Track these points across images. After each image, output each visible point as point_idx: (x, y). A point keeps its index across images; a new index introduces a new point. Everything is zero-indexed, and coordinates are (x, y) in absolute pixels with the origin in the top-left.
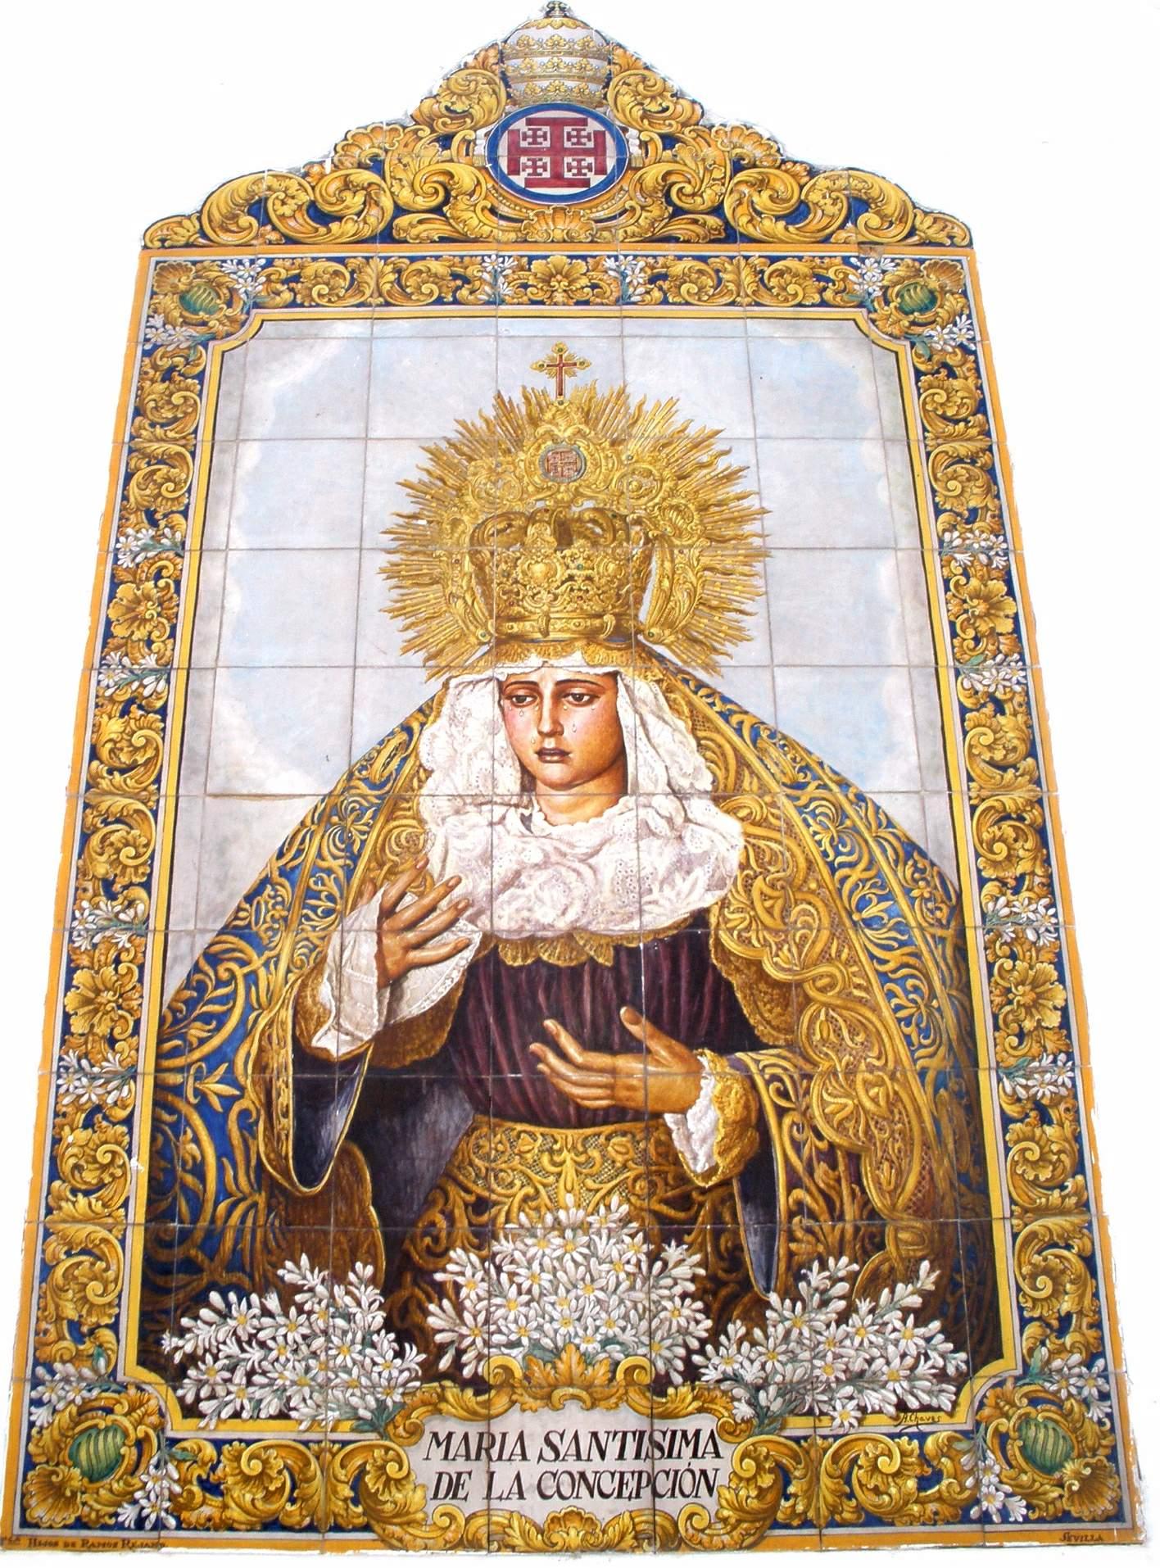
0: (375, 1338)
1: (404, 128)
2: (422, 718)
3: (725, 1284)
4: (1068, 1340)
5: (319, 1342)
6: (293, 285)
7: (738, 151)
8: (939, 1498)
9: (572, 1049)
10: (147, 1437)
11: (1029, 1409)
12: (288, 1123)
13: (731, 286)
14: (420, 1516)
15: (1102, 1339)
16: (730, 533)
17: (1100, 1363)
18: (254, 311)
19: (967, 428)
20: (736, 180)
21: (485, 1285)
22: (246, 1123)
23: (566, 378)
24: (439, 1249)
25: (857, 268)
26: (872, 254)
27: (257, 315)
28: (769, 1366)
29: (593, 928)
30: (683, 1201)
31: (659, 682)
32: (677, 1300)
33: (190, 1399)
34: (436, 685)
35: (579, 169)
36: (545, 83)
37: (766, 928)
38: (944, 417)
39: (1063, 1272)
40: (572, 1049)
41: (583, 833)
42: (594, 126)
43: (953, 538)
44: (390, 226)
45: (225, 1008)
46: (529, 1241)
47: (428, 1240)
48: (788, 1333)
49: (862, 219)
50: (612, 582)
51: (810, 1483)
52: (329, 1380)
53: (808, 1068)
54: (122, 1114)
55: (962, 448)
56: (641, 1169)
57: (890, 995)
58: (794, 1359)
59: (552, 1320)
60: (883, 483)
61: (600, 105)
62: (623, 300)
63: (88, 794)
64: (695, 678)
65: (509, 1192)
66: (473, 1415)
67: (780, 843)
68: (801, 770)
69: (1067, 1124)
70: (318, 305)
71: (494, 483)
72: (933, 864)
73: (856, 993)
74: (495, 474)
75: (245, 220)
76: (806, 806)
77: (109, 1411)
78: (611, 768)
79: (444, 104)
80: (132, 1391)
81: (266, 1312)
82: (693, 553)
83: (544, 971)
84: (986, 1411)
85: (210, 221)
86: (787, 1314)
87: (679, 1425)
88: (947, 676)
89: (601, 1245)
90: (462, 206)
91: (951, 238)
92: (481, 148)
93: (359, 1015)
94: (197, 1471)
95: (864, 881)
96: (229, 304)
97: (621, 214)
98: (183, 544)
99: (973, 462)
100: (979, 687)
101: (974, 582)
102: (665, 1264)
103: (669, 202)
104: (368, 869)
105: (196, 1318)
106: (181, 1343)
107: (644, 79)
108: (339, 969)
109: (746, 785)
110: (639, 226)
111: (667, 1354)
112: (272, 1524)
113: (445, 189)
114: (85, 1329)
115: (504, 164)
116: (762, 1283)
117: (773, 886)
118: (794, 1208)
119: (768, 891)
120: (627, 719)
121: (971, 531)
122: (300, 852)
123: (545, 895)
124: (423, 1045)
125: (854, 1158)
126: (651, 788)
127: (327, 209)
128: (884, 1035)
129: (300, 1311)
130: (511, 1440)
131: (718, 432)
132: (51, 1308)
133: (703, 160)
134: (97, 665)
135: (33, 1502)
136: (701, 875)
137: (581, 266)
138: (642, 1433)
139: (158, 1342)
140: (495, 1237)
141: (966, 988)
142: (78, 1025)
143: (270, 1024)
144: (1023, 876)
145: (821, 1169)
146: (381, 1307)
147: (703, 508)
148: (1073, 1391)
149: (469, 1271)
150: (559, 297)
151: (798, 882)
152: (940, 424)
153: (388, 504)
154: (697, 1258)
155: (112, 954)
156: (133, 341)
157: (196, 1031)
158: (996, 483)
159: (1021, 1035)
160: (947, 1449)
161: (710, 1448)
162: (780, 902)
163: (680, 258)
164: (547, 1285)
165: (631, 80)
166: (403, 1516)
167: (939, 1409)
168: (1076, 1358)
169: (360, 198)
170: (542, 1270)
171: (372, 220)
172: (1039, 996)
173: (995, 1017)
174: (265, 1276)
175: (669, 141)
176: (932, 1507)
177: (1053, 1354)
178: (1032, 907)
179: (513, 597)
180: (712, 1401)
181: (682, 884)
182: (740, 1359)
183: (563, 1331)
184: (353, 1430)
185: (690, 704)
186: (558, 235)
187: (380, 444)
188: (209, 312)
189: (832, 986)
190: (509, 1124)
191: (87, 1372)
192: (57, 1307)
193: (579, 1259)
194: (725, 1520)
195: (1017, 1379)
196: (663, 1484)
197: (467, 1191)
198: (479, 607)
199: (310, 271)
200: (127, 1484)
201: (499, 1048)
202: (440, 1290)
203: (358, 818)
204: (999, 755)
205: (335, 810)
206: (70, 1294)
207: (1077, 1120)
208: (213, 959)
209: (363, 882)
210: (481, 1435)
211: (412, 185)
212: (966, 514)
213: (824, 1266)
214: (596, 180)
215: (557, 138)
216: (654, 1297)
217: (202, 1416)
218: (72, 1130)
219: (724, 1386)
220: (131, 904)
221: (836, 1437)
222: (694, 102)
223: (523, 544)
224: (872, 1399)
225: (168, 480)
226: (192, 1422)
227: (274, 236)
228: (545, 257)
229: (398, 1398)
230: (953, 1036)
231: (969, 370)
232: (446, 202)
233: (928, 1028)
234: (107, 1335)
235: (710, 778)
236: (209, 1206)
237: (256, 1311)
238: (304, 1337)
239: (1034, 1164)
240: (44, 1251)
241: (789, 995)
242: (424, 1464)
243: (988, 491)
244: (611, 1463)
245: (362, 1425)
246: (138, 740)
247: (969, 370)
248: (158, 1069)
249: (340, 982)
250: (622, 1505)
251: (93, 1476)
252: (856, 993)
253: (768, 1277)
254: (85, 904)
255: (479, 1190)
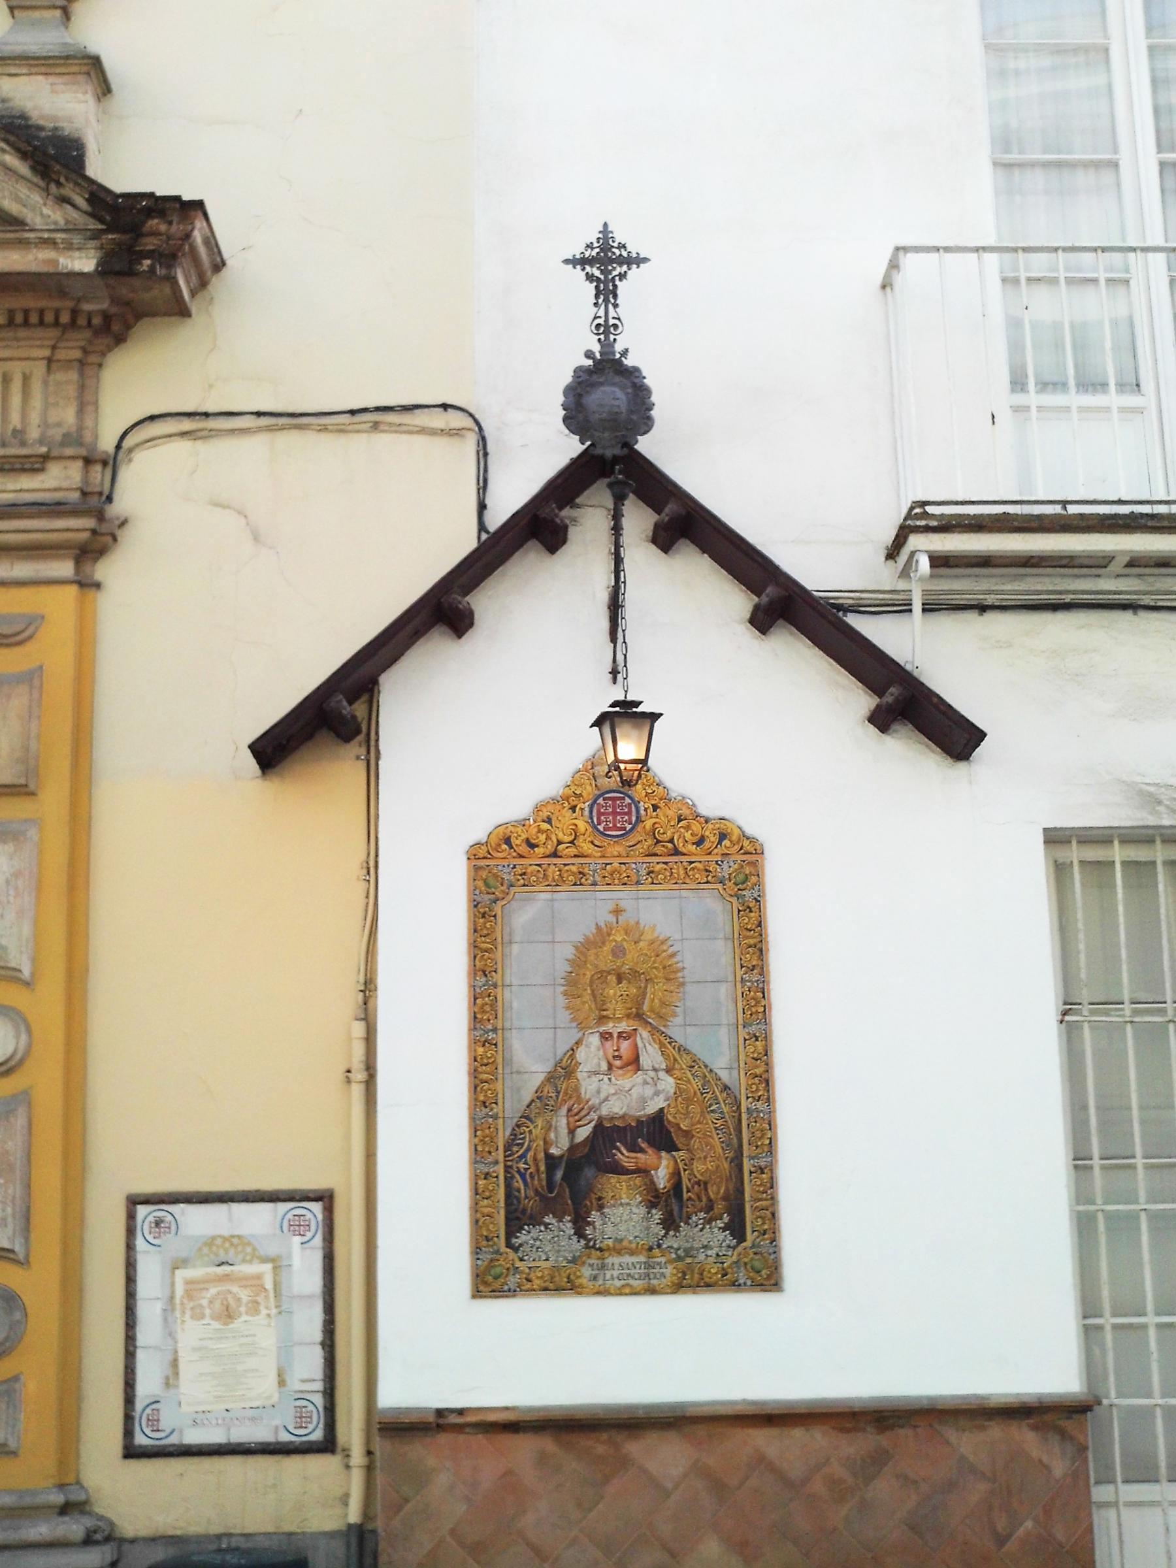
9: (625, 1152)
12: (544, 1176)
27: (513, 890)
34: (580, 1034)
40: (625, 1152)
43: (746, 977)
55: (752, 941)
62: (638, 883)
63: (474, 1073)
74: (597, 955)
75: (505, 846)
78: (634, 1062)
92: (586, 813)
112: (546, 1289)
120: (640, 1044)
125: (706, 1183)
136: (662, 1097)
145: (696, 1187)
153: (562, 968)
156: (469, 901)
157: (515, 1149)
166: (581, 1286)
169: (544, 836)
179: (604, 1003)
181: (656, 1099)
186: (616, 853)
196: (652, 1276)
198: (593, 1006)
202: (589, 1224)
205: (552, 1077)
208: (518, 1126)
224: (709, 1253)
241: (688, 1134)
242: (587, 1272)
245: (569, 1262)
251: (496, 1278)
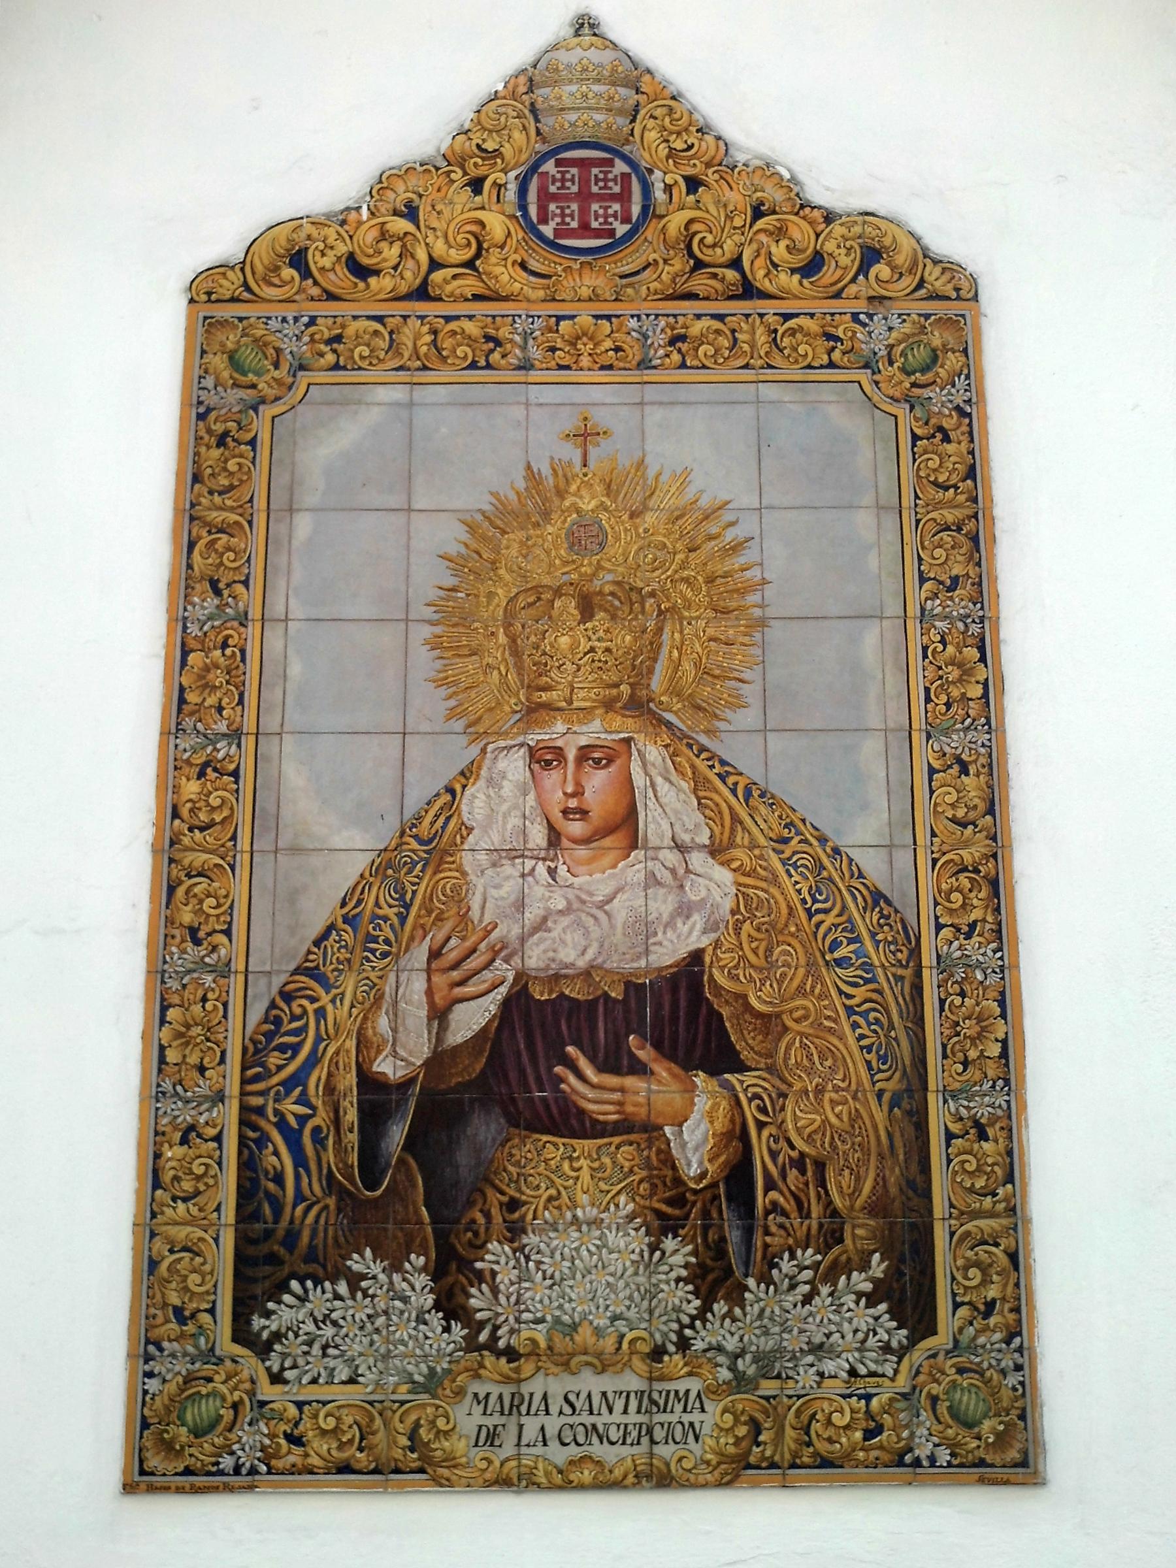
0: (427, 1316)
1: (437, 169)
2: (463, 781)
3: (713, 1270)
4: (992, 1321)
5: (381, 1321)
6: (335, 346)
7: (759, 194)
8: (881, 1447)
10: (241, 1400)
11: (957, 1377)
12: (353, 1138)
13: (746, 347)
14: (464, 1460)
15: (1019, 1321)
16: (734, 604)
17: (1017, 1340)
18: (300, 373)
19: (956, 494)
20: (755, 228)
21: (516, 1272)
22: (318, 1138)
23: (590, 448)
24: (479, 1243)
25: (864, 325)
26: (881, 309)
27: (304, 378)
28: (746, 1338)
29: (607, 966)
30: (678, 1201)
31: (666, 746)
32: (673, 1284)
33: (276, 1369)
34: (475, 750)
35: (606, 217)
36: (573, 117)
37: (752, 966)
38: (935, 484)
39: (990, 1265)
40: (589, 1072)
41: (600, 883)
42: (620, 167)
43: (935, 606)
44: (425, 282)
45: (297, 1039)
46: (552, 1235)
47: (470, 1234)
48: (762, 1311)
49: (873, 271)
50: (628, 653)
51: (777, 1434)
52: (389, 1351)
53: (784, 1087)
54: (211, 1132)
55: (950, 516)
56: (644, 1173)
57: (855, 1026)
58: (766, 1333)
59: (571, 1300)
60: (875, 551)
61: (627, 142)
62: (644, 364)
64: (697, 742)
65: (536, 1195)
66: (506, 1380)
67: (766, 891)
68: (786, 826)
69: (1001, 1140)
70: (360, 368)
71: (525, 557)
72: (896, 911)
73: (826, 1023)
74: (526, 548)
75: (288, 273)
76: (789, 859)
77: (209, 1380)
78: (624, 827)
79: (474, 142)
80: (228, 1363)
81: (337, 1297)
82: (701, 624)
83: (566, 1004)
84: (921, 1378)
85: (253, 273)
86: (762, 1295)
87: (672, 1386)
88: (918, 738)
89: (611, 1237)
90: (493, 260)
91: (957, 290)
92: (511, 194)
93: (412, 1043)
94: (283, 1427)
95: (836, 926)
96: (276, 366)
97: (644, 269)
98: (246, 613)
99: (959, 530)
100: (947, 749)
101: (950, 649)
102: (663, 1253)
103: (691, 254)
104: (419, 916)
105: (279, 1302)
106: (267, 1323)
107: (671, 110)
108: (395, 1003)
109: (738, 840)
110: (661, 282)
111: (664, 1328)
112: (345, 1468)
113: (477, 238)
114: (187, 1313)
115: (533, 211)
116: (742, 1269)
117: (758, 930)
118: (769, 1207)
119: (754, 934)
120: (639, 779)
121: (951, 599)
122: (359, 902)
123: (568, 938)
124: (465, 1069)
125: (820, 1166)
126: (657, 843)
127: (365, 261)
128: (849, 1060)
129: (365, 1295)
130: (537, 1398)
131: (728, 503)
132: (158, 1296)
133: (725, 206)
134: (173, 730)
135: (148, 1455)
137: (605, 326)
138: (643, 1392)
139: (249, 1322)
140: (525, 1232)
141: (920, 1021)
142: (172, 1056)
143: (337, 1053)
144: (975, 922)
145: (793, 1174)
146: (431, 1291)
147: (710, 580)
148: (994, 1363)
149: (503, 1260)
150: (585, 361)
151: (780, 926)
152: (931, 490)
153: (431, 578)
154: (690, 1247)
155: (200, 993)
156: (185, 404)
157: (274, 1059)
158: (978, 551)
159: (966, 1063)
160: (887, 1409)
161: (697, 1405)
162: (764, 944)
163: (698, 317)
164: (566, 1271)
165: (658, 112)
166: (450, 1461)
167: (883, 1375)
168: (998, 1336)
169: (396, 250)
170: (563, 1259)
171: (408, 275)
172: (983, 1029)
173: (944, 1046)
174: (335, 1266)
175: (693, 184)
176: (874, 1454)
177: (979, 1332)
178: (982, 951)
179: (542, 669)
180: (700, 1367)
181: (682, 927)
182: (722, 1332)
183: (579, 1309)
184: (409, 1392)
185: (693, 766)
186: (585, 292)
187: (423, 515)
188: (258, 374)
189: (806, 1017)
190: (537, 1136)
191: (190, 1349)
192: (163, 1295)
193: (593, 1249)
194: (708, 1463)
195: (948, 1352)
196: (659, 1434)
197: (503, 1193)
199: (350, 331)
200: (226, 1439)
201: (529, 1070)
202: (480, 1276)
203: (410, 871)
204: (960, 813)
206: (174, 1285)
207: (1010, 1138)
209: (414, 928)
210: (513, 1395)
211: (446, 236)
212: (948, 582)
213: (793, 1257)
214: (621, 229)
215: (584, 182)
216: (654, 1281)
217: (286, 1382)
218: (171, 1147)
219: (709, 1355)
220: (214, 948)
221: (799, 1397)
222: (719, 138)
223: (550, 617)
224: (829, 1366)
225: (229, 549)
226: (279, 1388)
227: (315, 291)
228: (572, 317)
229: (445, 1366)
230: (907, 1062)
231: (963, 434)
232: (478, 255)
233: (886, 1054)
234: (205, 1318)
235: (708, 833)
236: (288, 1210)
237: (329, 1295)
238: (369, 1316)
239: (971, 1174)
240: (150, 1249)
241: (770, 1024)
243: (971, 558)
244: (617, 1417)
245: (416, 1387)
246: (214, 801)
247: (963, 434)
248: (243, 1093)
249: (396, 1015)
250: (626, 1451)
251: (198, 1433)
252: (826, 1023)
253: (747, 1264)
254: (174, 949)
255: (512, 1192)
